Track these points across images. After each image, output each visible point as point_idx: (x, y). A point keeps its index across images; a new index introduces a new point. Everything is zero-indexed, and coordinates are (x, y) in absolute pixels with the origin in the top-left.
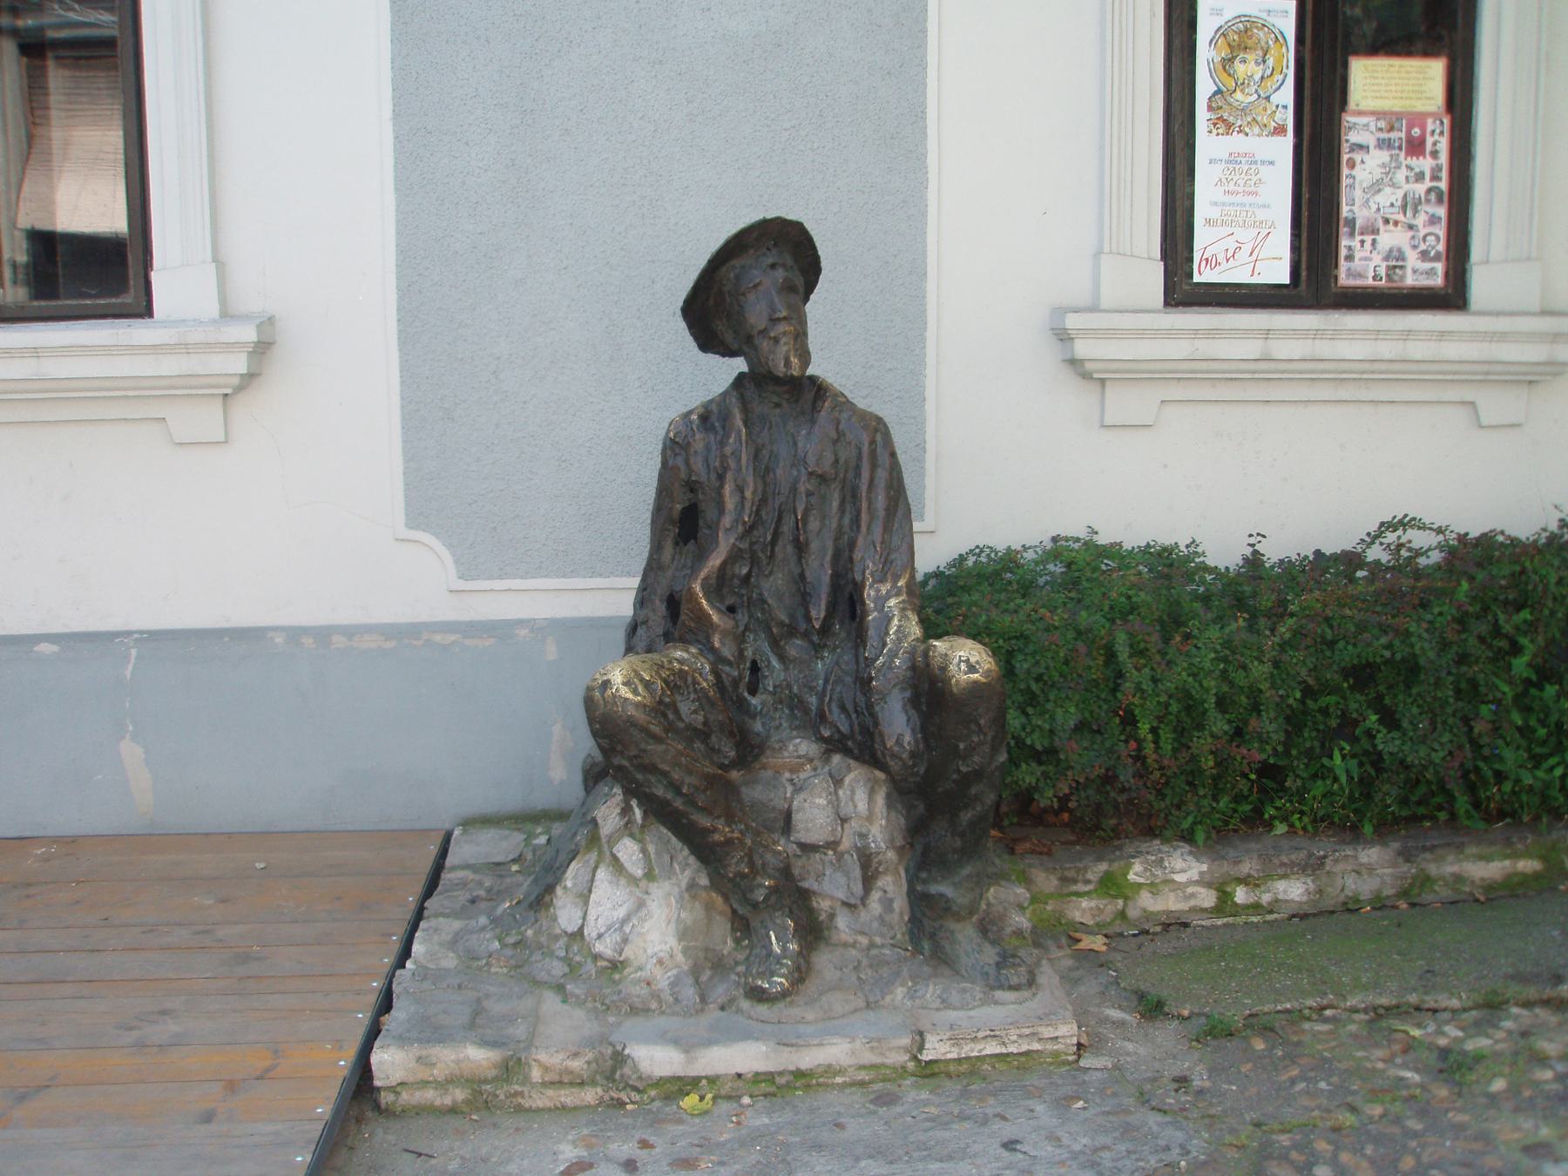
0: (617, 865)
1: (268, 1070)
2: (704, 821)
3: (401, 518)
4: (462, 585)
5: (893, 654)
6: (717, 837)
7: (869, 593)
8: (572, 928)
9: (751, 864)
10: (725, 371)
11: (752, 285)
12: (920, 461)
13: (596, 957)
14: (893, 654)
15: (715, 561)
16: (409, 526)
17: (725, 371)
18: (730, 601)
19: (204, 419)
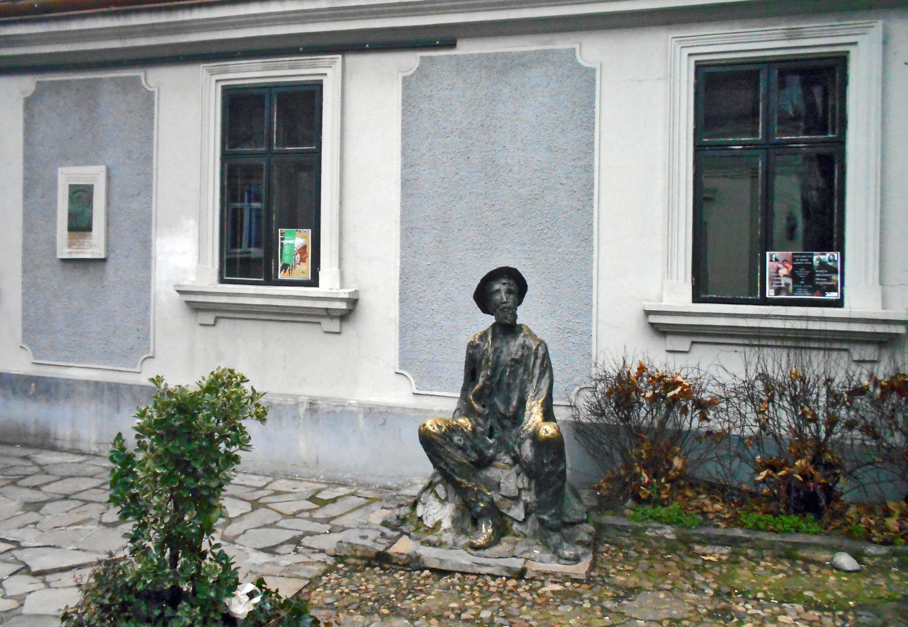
0: (437, 496)
1: (276, 522)
2: (458, 479)
3: (397, 365)
4: (416, 392)
5: (530, 427)
6: (463, 486)
7: (528, 404)
8: (419, 515)
9: (477, 498)
10: (490, 320)
11: (500, 291)
12: (195, 287)
13: (425, 526)
14: (530, 427)
15: (477, 387)
16: (400, 368)
17: (490, 320)
18: (483, 403)
19: (334, 325)
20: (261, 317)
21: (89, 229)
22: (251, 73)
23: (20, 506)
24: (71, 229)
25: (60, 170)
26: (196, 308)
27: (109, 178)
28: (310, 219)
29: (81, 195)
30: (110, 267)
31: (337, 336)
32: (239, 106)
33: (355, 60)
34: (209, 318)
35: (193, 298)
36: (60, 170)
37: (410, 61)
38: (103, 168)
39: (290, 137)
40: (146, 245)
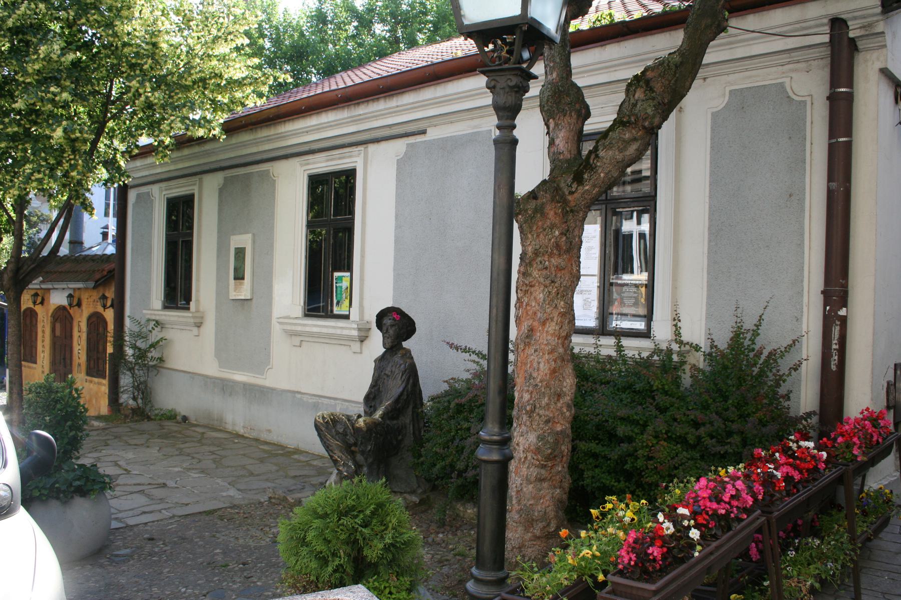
20: (603, 65)
21: (243, 278)
22: (322, 164)
23: (784, 366)
24: (235, 279)
25: (232, 237)
26: (292, 334)
27: (254, 242)
28: (349, 268)
29: (240, 253)
30: (254, 300)
31: (359, 355)
32: (316, 182)
33: (372, 148)
34: (297, 341)
35: (289, 327)
36: (232, 237)
37: (400, 145)
38: (250, 235)
39: (319, 244)
40: (270, 288)
